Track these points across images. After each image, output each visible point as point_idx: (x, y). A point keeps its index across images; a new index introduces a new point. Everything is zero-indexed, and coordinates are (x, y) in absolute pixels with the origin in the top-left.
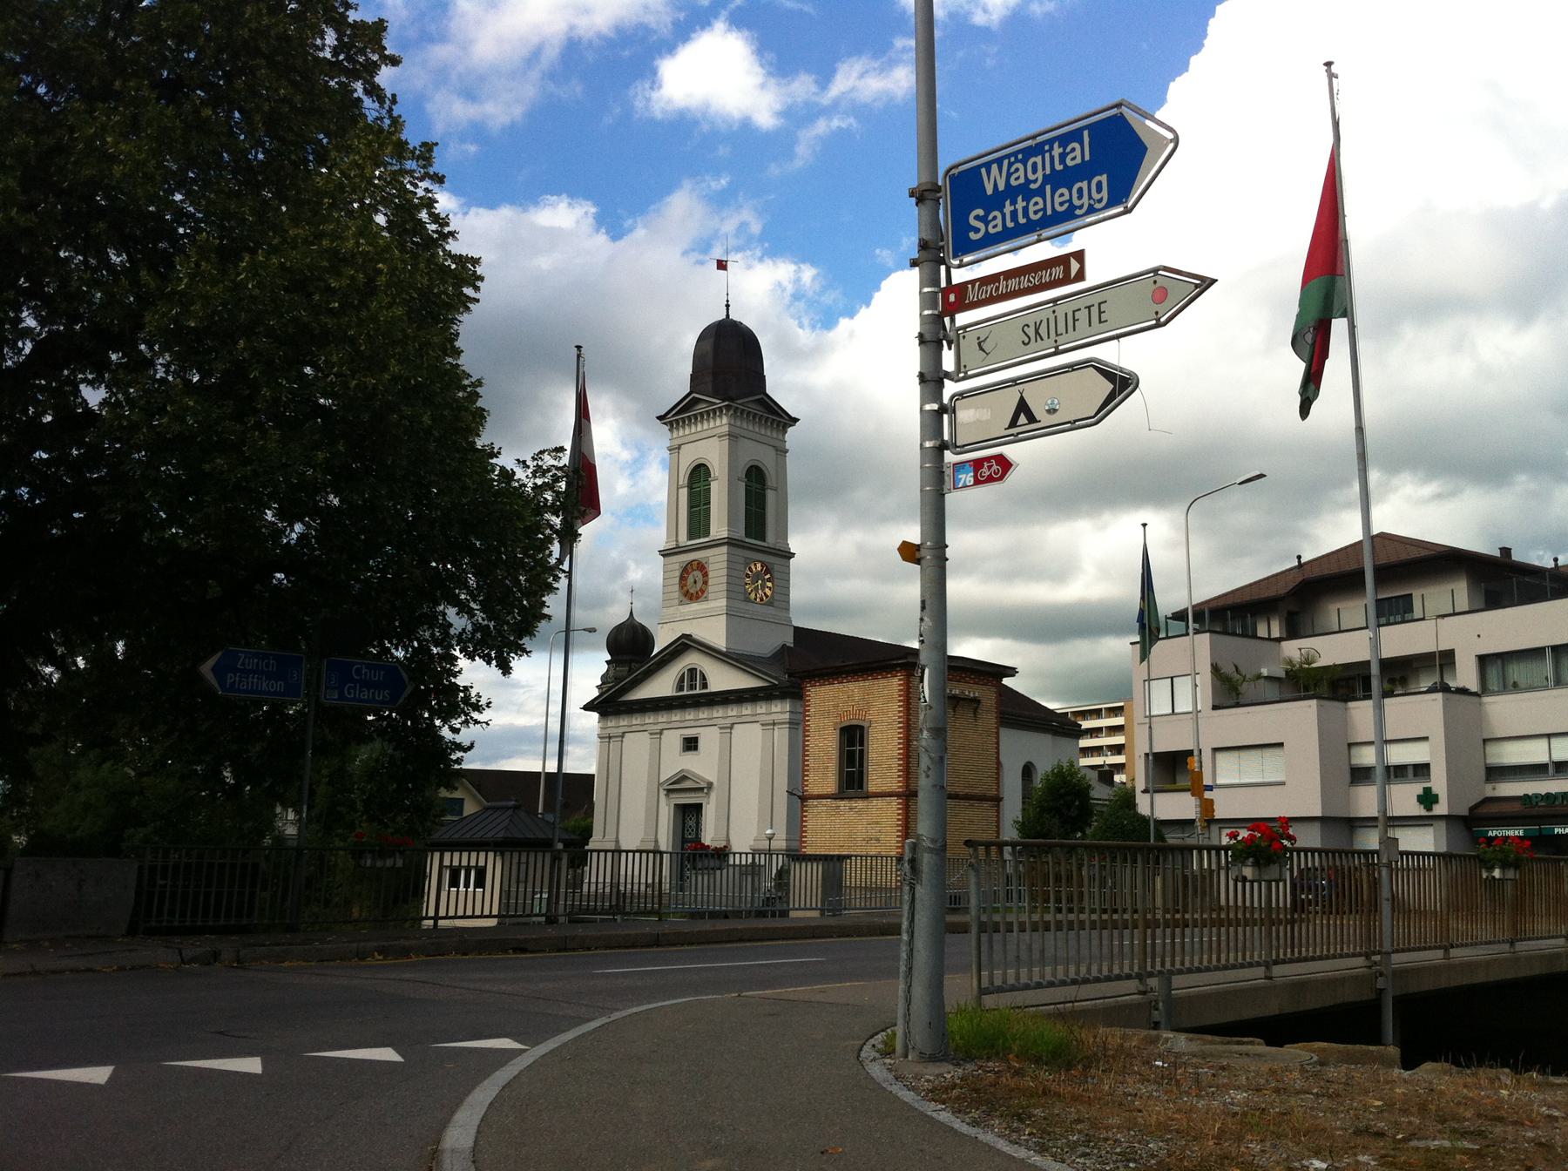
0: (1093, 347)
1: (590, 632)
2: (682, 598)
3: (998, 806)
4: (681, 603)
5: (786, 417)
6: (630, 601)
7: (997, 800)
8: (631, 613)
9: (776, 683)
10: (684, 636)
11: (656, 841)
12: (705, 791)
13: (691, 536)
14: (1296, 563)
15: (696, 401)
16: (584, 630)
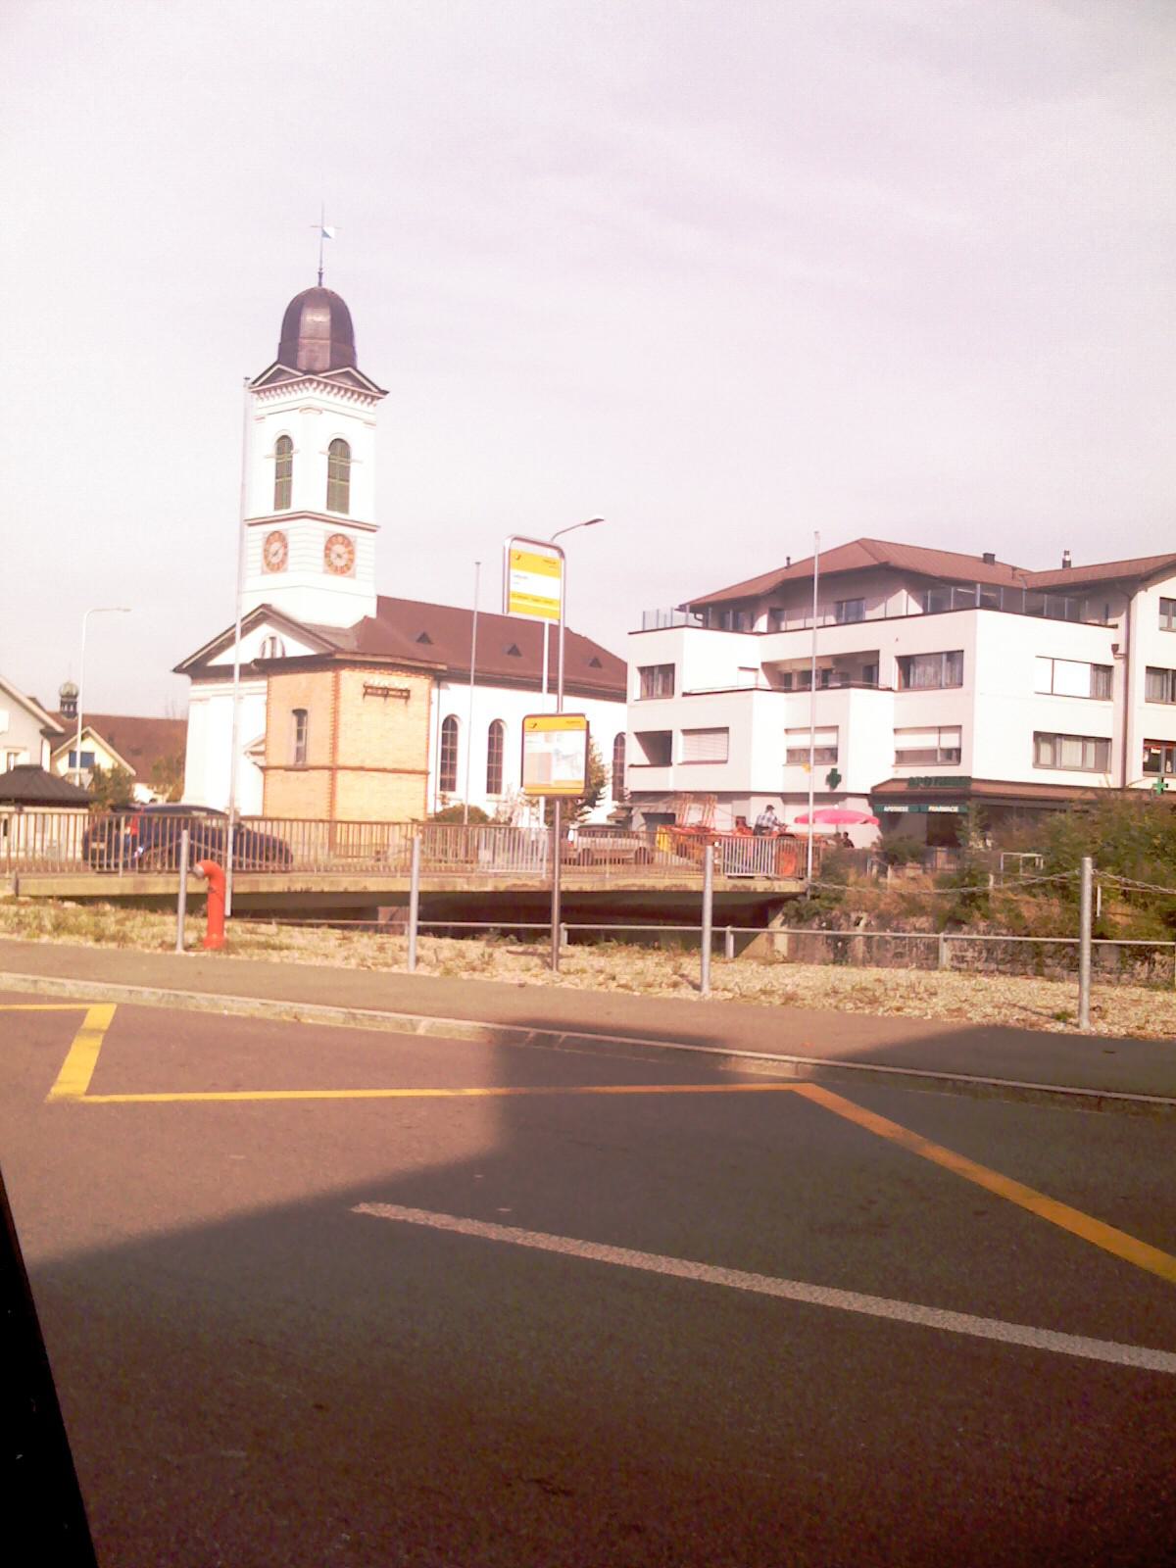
2: (265, 568)
3: (427, 778)
4: (263, 573)
7: (426, 773)
13: (278, 506)
14: (785, 565)
15: (280, 372)
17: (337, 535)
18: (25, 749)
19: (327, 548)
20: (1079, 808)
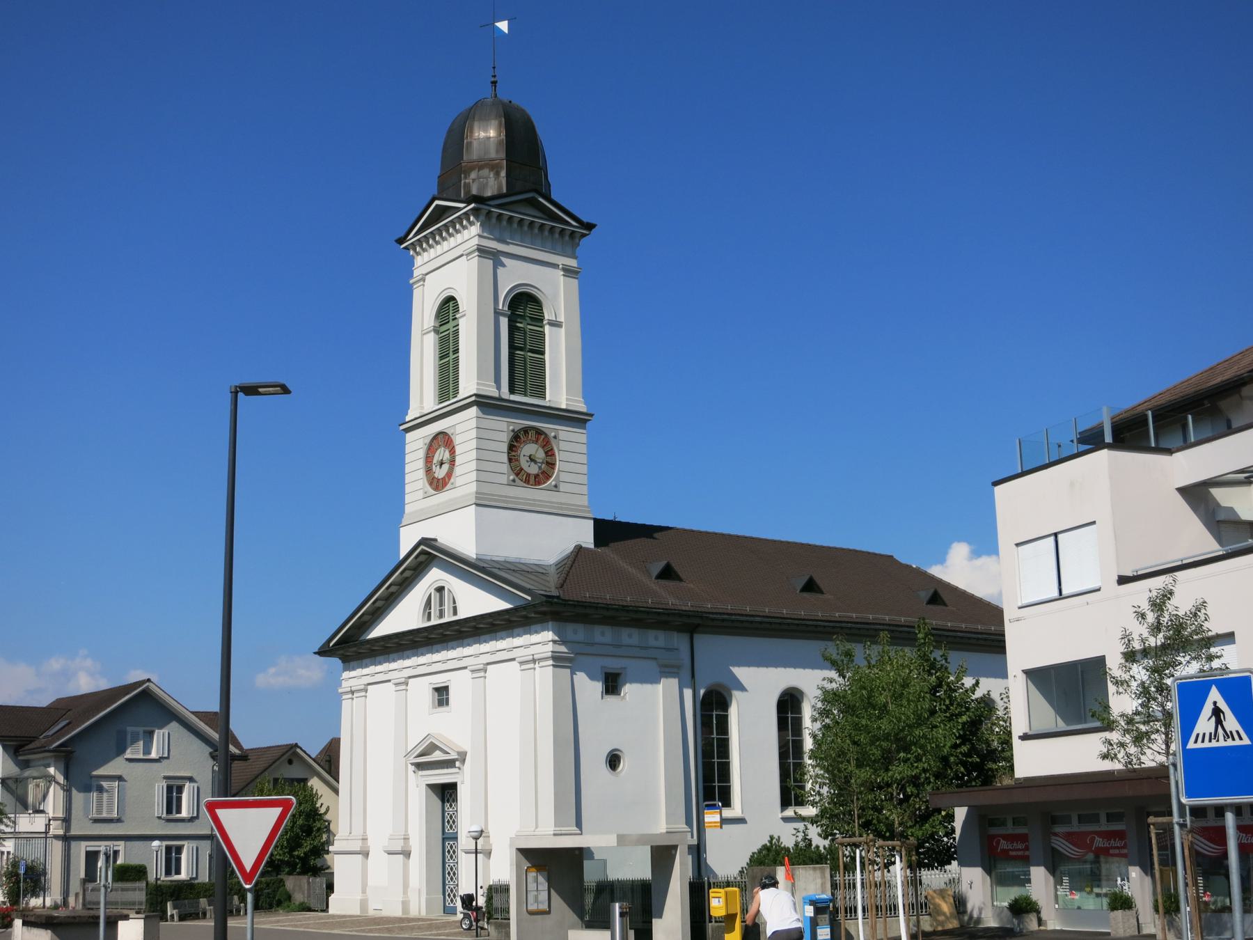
0: (1239, 434)
5: (574, 223)
9: (529, 598)
10: (424, 541)
11: (406, 839)
12: (457, 764)
17: (526, 430)
18: (191, 779)
19: (511, 448)
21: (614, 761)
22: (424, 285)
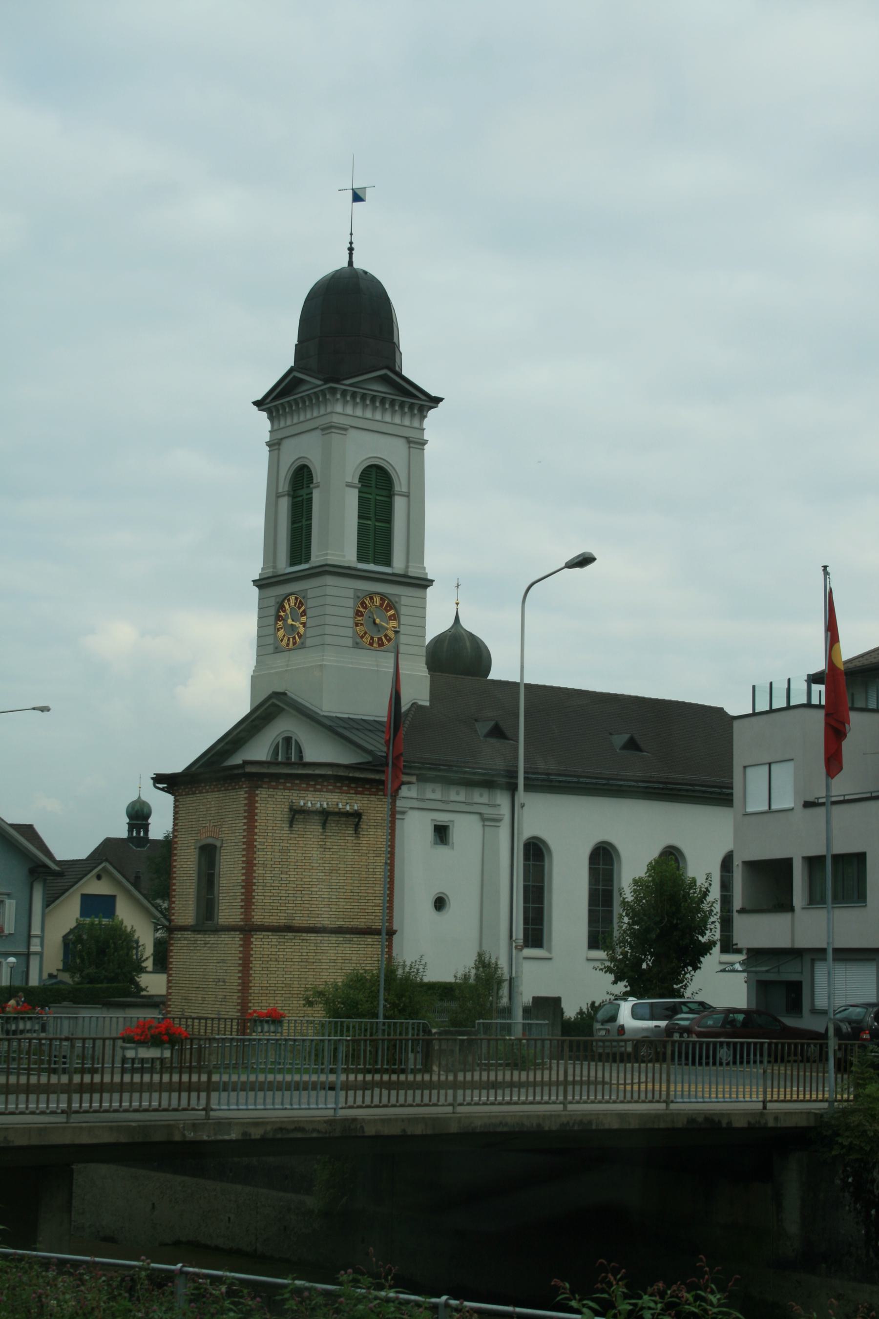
1: (42, 711)
5: (423, 397)
6: (455, 601)
8: (457, 618)
13: (294, 560)
16: (34, 709)
20: (277, 1057)
21: (440, 903)
22: (279, 449)
